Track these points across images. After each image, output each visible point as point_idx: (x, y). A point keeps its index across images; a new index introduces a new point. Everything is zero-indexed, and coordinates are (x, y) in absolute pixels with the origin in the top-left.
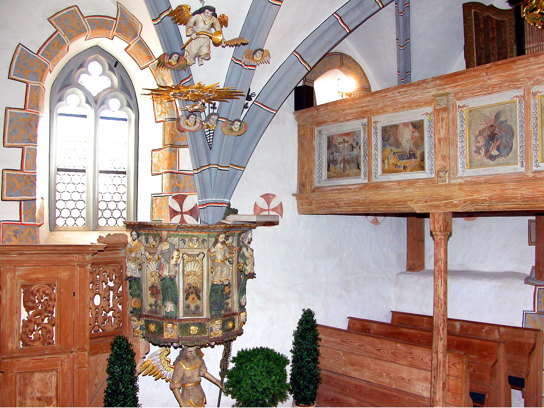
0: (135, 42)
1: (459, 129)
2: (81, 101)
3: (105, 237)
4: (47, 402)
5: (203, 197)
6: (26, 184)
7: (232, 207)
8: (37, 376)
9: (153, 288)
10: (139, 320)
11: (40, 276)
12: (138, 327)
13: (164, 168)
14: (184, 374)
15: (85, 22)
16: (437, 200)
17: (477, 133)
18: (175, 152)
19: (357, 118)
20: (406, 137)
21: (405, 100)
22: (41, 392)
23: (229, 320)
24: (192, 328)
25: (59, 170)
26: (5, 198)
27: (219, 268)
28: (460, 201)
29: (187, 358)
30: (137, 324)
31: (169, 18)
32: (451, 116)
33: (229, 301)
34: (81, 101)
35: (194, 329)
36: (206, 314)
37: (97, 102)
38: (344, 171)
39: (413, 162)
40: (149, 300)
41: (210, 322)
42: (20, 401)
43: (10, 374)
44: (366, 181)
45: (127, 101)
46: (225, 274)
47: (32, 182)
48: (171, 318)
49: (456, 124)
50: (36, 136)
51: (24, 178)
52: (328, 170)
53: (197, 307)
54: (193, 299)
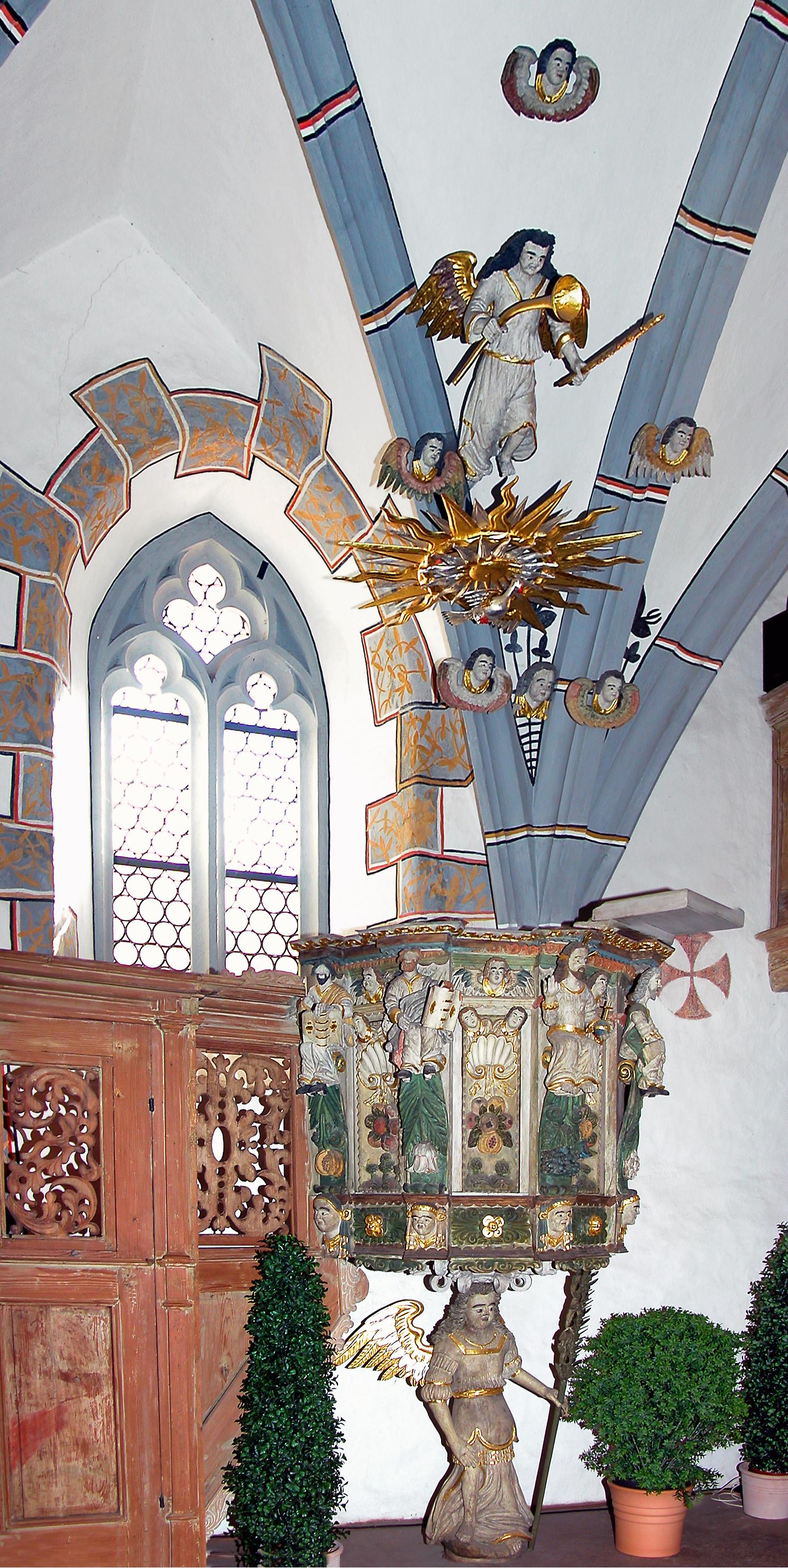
0: (314, 473)
2: (171, 673)
4: (88, 1388)
5: (513, 916)
9: (377, 1119)
10: (339, 1209)
12: (334, 1226)
13: (403, 843)
14: (461, 1366)
15: (171, 408)
18: (432, 796)
23: (588, 1213)
24: (488, 1220)
25: (118, 860)
27: (570, 1045)
29: (468, 1327)
30: (333, 1219)
33: (590, 1161)
34: (171, 673)
35: (492, 1227)
36: (527, 1186)
37: (219, 677)
40: (365, 1153)
41: (537, 1208)
42: (14, 1377)
45: (296, 677)
46: (583, 1069)
47: (42, 851)
48: (429, 1191)
50: (48, 727)
51: (21, 840)
54: (492, 1143)
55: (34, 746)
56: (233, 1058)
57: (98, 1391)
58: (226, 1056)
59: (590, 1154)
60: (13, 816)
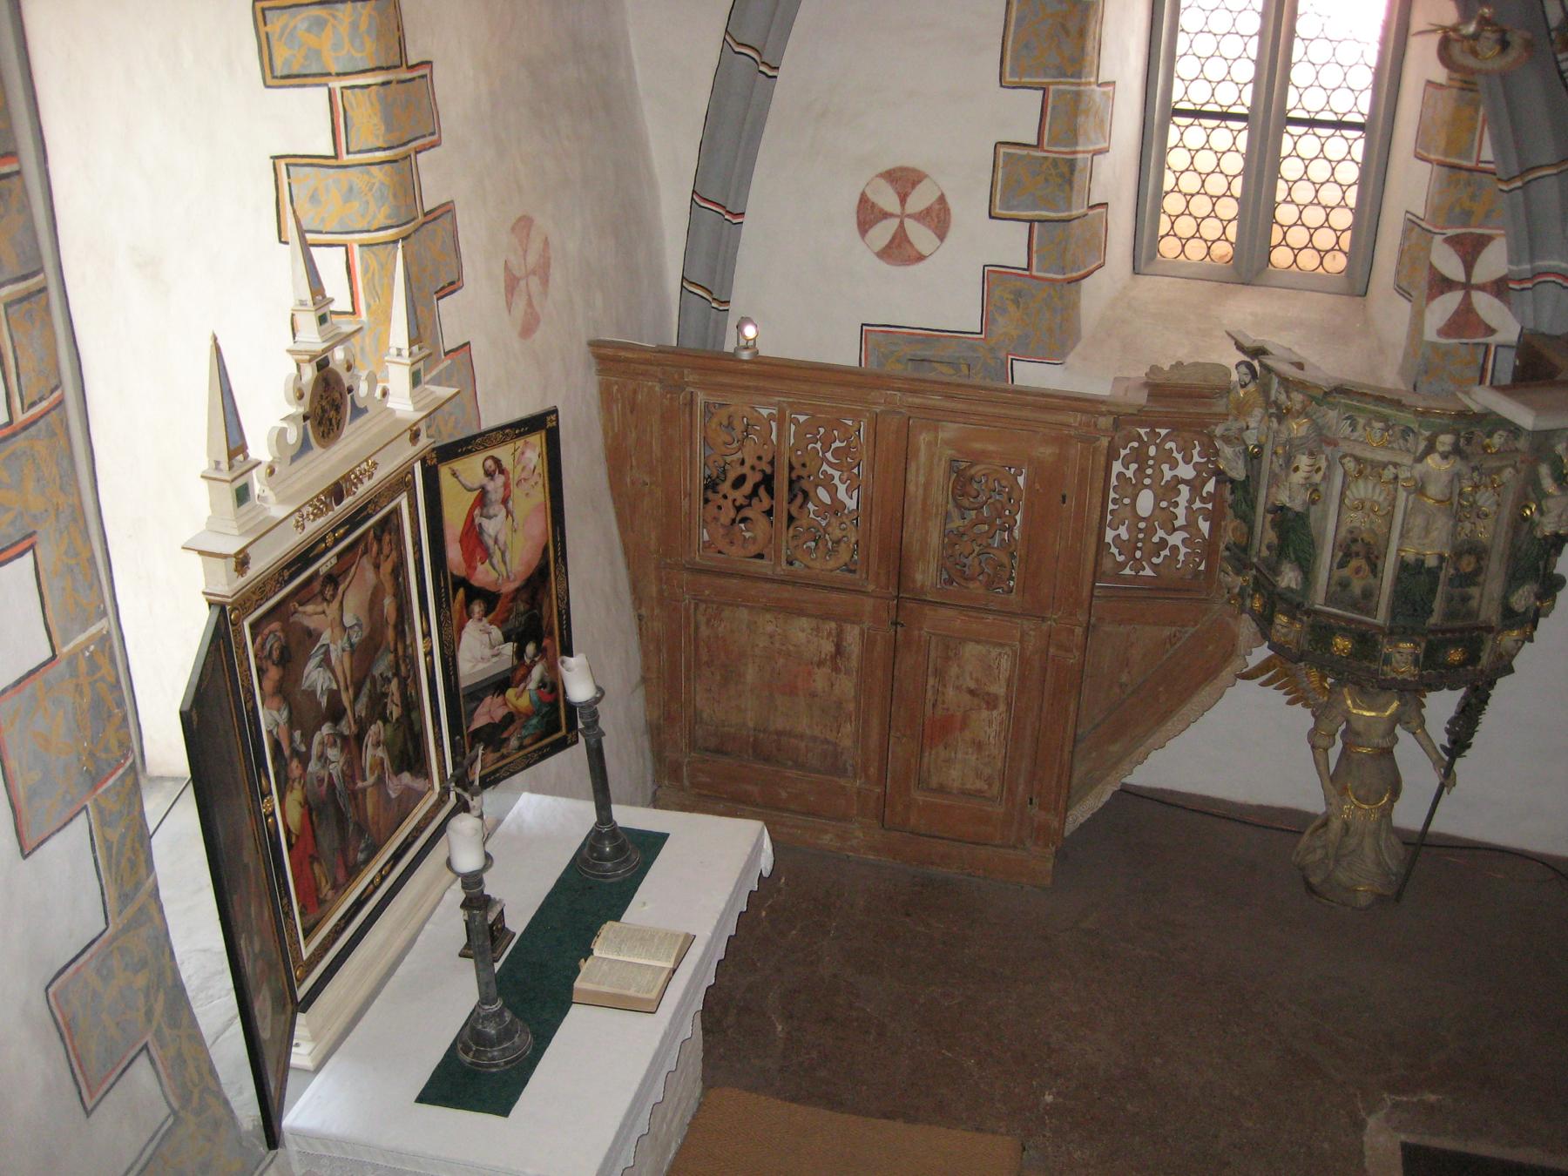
3: (1166, 368)
4: (988, 703)
6: (1046, 180)
8: (971, 650)
11: (991, 447)
22: (977, 680)
26: (998, 211)
33: (1474, 591)
35: (1342, 644)
36: (1381, 618)
43: (916, 632)
53: (1368, 594)
56: (1163, 432)
57: (995, 707)
59: (1475, 584)
60: (1039, 145)
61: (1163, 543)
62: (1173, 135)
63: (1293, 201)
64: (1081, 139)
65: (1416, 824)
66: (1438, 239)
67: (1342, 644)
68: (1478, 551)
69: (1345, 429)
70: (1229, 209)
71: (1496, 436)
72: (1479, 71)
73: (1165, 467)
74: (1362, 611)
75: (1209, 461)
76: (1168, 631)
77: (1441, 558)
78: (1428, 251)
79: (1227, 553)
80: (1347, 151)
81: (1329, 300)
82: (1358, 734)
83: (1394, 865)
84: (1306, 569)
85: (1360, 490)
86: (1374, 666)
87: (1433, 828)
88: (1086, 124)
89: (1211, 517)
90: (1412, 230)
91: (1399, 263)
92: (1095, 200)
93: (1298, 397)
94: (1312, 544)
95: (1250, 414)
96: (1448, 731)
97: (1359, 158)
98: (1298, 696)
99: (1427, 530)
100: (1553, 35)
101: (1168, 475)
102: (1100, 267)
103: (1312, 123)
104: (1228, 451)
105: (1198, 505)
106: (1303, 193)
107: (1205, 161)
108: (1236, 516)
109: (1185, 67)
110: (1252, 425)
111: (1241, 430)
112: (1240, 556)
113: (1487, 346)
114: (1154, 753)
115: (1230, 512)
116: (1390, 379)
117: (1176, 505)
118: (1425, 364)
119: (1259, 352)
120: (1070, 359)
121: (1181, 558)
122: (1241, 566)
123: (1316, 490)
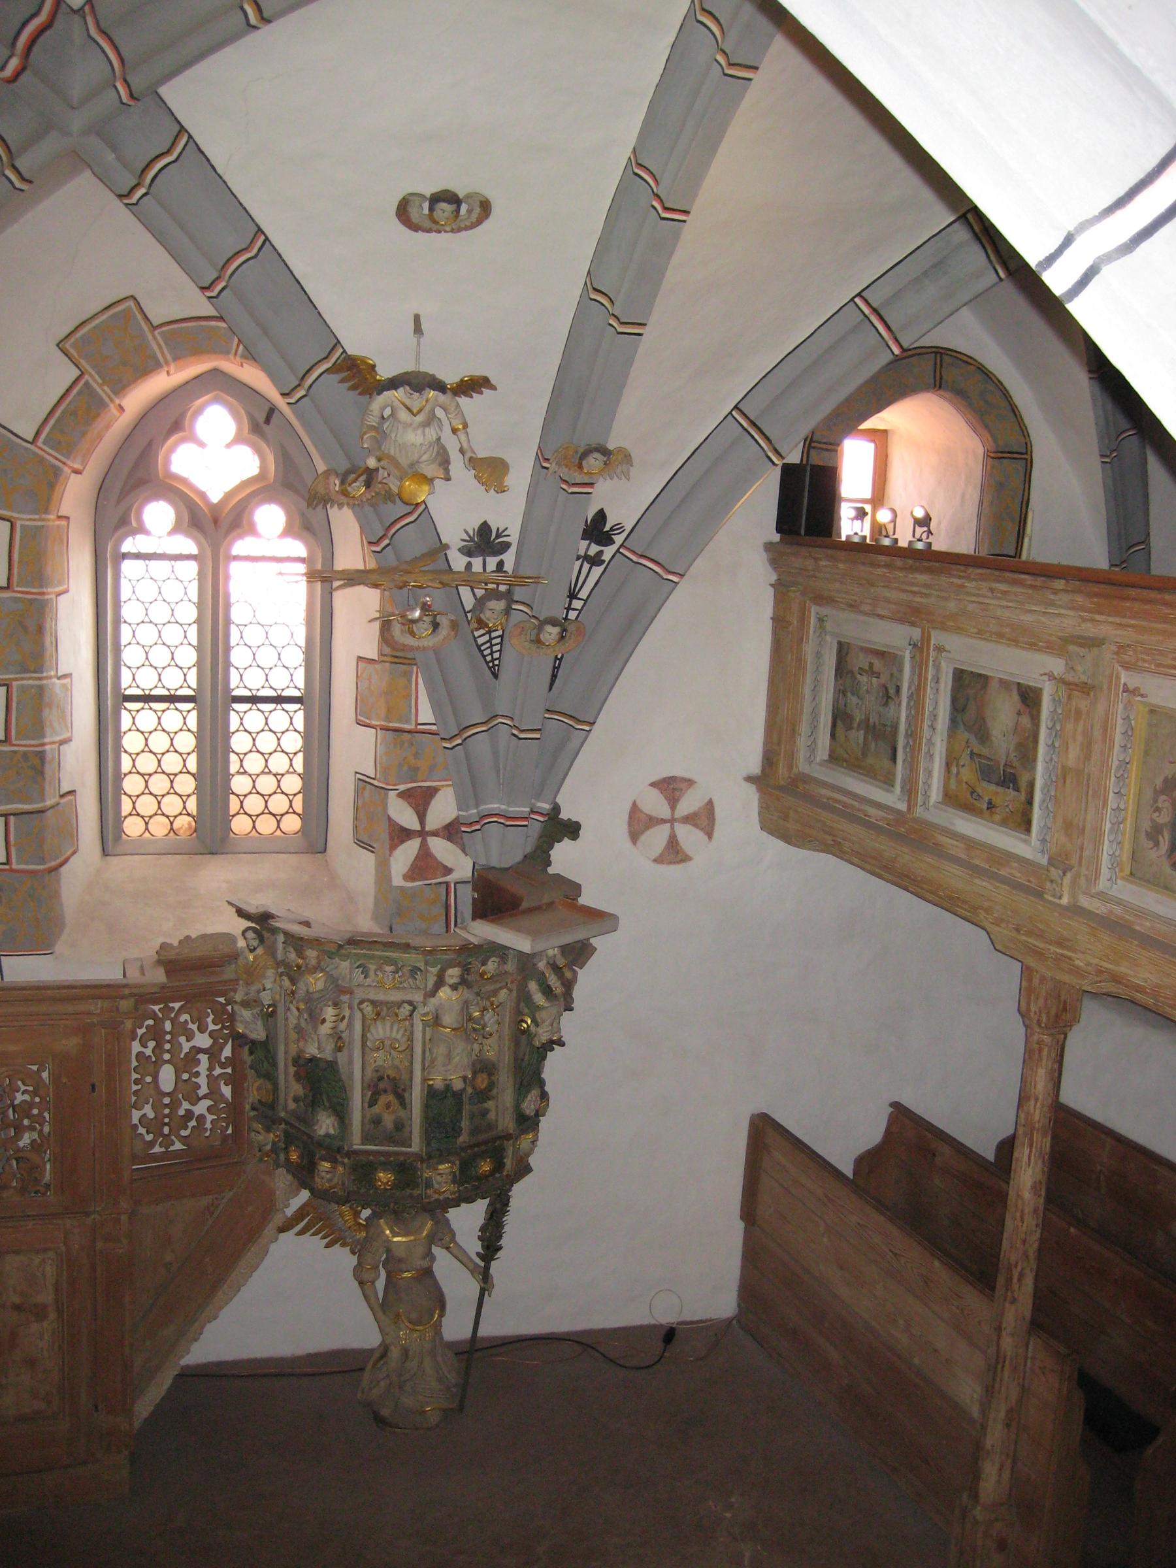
1: (1116, 755)
3: (176, 944)
6: (18, 773)
7: (564, 815)
11: (12, 1048)
16: (1041, 936)
17: (1159, 782)
19: (901, 621)
20: (1003, 714)
21: (1006, 614)
28: (1089, 964)
31: (334, 378)
32: (1100, 709)
33: (490, 1104)
35: (384, 1177)
36: (416, 1145)
38: (864, 755)
39: (1007, 798)
44: (902, 807)
49: (1112, 741)
52: (833, 735)
53: (399, 1126)
55: (28, 675)
56: (177, 1005)
57: (45, 1317)
58: (171, 1005)
61: (189, 1114)
62: (126, 720)
63: (245, 772)
64: (48, 731)
65: (465, 1333)
66: (392, 794)
67: (384, 1177)
68: (484, 1067)
69: (358, 975)
70: (186, 784)
71: (490, 963)
72: (418, 648)
73: (182, 1039)
74: (396, 1144)
75: (224, 1027)
76: (205, 1201)
77: (465, 1078)
78: (385, 808)
79: (252, 1114)
80: (289, 724)
81: (293, 859)
82: (400, 1260)
83: (452, 1378)
84: (341, 1113)
85: (380, 1031)
86: (416, 1192)
87: (482, 1333)
88: (51, 716)
89: (230, 1080)
90: (364, 789)
91: (356, 818)
92: (65, 788)
93: (311, 954)
94: (343, 1088)
95: (264, 976)
96: (480, 1238)
97: (301, 728)
98: (335, 1238)
99: (449, 1057)
100: (469, 615)
101: (186, 1047)
102: (74, 852)
103: (254, 700)
104: (246, 1014)
105: (218, 1071)
106: (254, 764)
107: (159, 742)
108: (259, 1075)
109: (131, 656)
110: (268, 986)
111: (259, 992)
112: (267, 1112)
113: (447, 884)
114: (208, 1326)
115: (250, 1073)
116: (366, 923)
117: (197, 1074)
118: (394, 905)
119: (263, 918)
120: (59, 948)
121: (208, 1125)
122: (270, 1122)
123: (340, 1038)
